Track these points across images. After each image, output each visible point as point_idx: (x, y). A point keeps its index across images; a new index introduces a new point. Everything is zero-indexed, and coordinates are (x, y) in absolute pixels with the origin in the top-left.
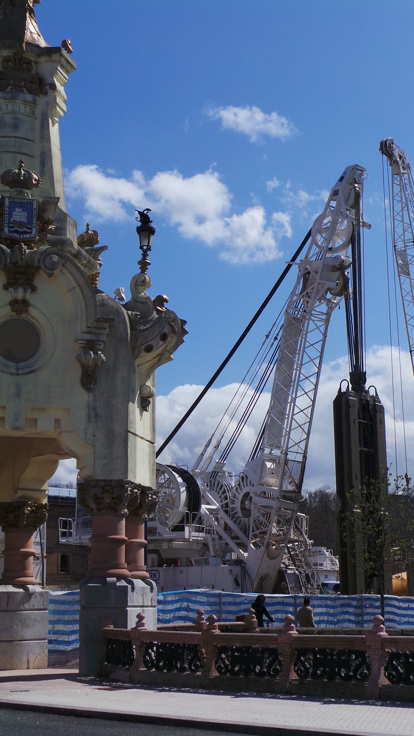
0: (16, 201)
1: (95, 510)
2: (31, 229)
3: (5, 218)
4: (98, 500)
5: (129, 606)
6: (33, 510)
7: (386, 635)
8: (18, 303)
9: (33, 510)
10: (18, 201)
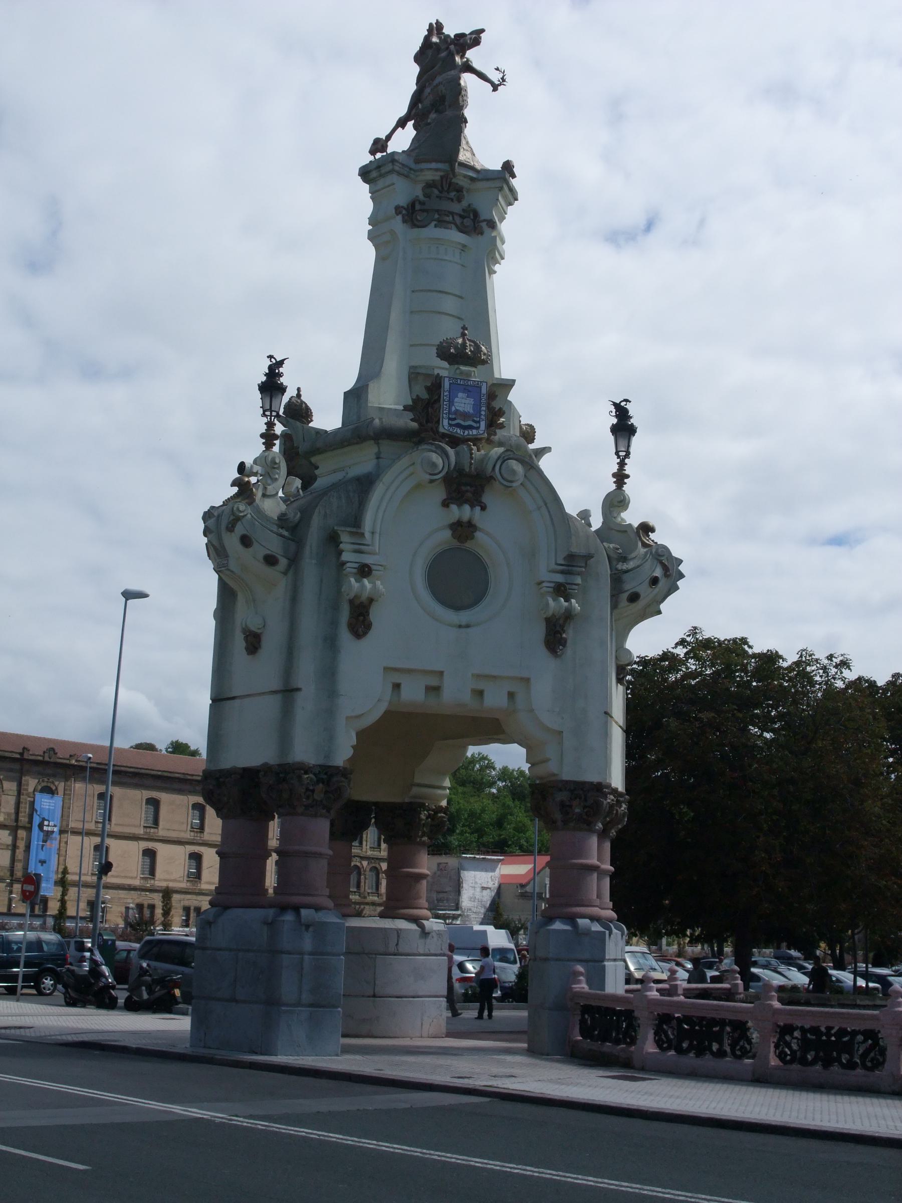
0: (459, 382)
1: (560, 823)
2: (479, 422)
3: (445, 406)
4: (565, 808)
5: (609, 960)
6: (429, 814)
7: (657, 995)
8: (462, 526)
9: (429, 814)
10: (462, 383)
